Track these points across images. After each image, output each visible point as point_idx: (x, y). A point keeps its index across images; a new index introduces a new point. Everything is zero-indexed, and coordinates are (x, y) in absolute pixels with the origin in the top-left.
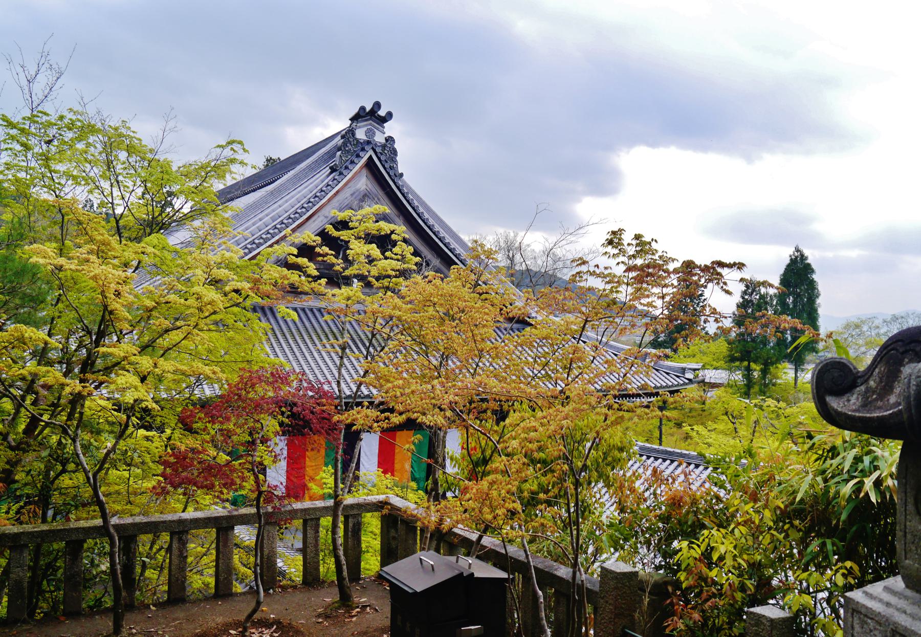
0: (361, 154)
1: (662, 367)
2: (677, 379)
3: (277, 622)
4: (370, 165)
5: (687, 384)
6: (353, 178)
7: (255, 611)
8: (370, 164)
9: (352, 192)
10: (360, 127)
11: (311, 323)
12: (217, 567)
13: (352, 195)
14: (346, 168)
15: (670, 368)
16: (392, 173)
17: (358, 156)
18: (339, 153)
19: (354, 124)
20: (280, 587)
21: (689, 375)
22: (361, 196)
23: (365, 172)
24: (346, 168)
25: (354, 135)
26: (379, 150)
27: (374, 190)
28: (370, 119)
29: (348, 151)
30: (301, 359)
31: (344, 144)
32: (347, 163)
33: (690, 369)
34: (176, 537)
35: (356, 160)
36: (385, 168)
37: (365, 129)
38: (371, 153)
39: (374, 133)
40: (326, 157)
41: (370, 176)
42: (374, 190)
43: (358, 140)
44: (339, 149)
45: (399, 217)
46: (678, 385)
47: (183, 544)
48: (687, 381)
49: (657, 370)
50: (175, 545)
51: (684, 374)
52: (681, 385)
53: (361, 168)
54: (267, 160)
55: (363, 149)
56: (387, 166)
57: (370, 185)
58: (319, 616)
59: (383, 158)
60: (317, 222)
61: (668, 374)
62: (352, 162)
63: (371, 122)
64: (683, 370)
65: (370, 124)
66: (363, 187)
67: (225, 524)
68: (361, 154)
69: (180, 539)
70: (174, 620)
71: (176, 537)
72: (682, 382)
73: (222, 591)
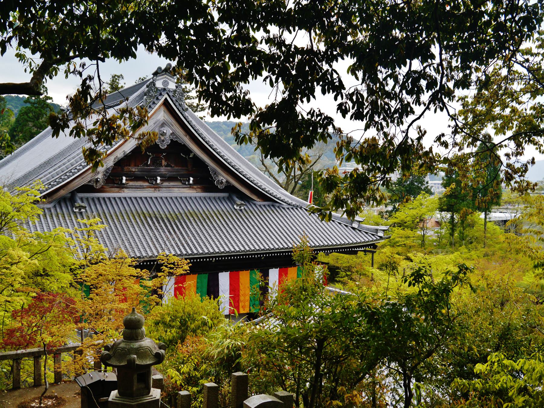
0: (160, 97)
1: (363, 228)
2: (373, 237)
3: (56, 397)
4: (166, 104)
5: (378, 240)
6: (155, 112)
7: (45, 392)
8: (166, 103)
9: (154, 122)
10: (158, 80)
11: (130, 207)
12: (34, 373)
13: (154, 124)
14: (150, 107)
15: (368, 229)
16: (180, 108)
17: (157, 99)
18: (145, 97)
19: (155, 78)
20: (64, 381)
21: (381, 234)
22: (160, 124)
23: (163, 108)
24: (150, 107)
25: (154, 85)
26: (171, 94)
27: (169, 120)
28: (165, 74)
29: (151, 96)
30: (128, 223)
31: (149, 91)
32: (151, 104)
33: (381, 230)
34: (15, 361)
35: (156, 102)
36: (176, 106)
37: (162, 80)
38: (166, 96)
39: (168, 83)
40: (137, 99)
41: (166, 110)
42: (169, 120)
43: (157, 89)
44: (145, 95)
45: (186, 136)
46: (372, 241)
47: (18, 364)
48: (378, 238)
49: (360, 231)
50: (15, 365)
51: (377, 233)
52: (375, 241)
53: (160, 106)
54: (113, 77)
55: (161, 94)
56: (177, 104)
57: (166, 117)
58: (75, 394)
59: (174, 99)
60: (131, 143)
61: (366, 233)
62: (154, 103)
63: (165, 76)
64: (377, 231)
65: (166, 77)
66: (163, 118)
67: (37, 355)
68: (160, 97)
69: (17, 362)
70: (14, 396)
71: (15, 361)
72: (375, 239)
73: (37, 383)
